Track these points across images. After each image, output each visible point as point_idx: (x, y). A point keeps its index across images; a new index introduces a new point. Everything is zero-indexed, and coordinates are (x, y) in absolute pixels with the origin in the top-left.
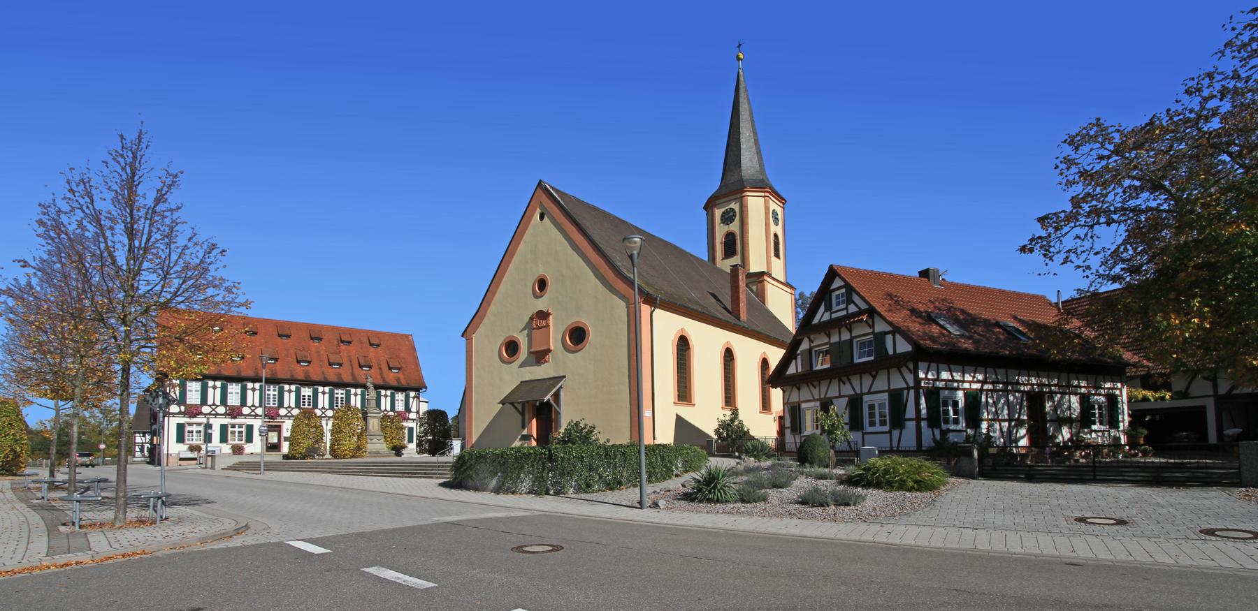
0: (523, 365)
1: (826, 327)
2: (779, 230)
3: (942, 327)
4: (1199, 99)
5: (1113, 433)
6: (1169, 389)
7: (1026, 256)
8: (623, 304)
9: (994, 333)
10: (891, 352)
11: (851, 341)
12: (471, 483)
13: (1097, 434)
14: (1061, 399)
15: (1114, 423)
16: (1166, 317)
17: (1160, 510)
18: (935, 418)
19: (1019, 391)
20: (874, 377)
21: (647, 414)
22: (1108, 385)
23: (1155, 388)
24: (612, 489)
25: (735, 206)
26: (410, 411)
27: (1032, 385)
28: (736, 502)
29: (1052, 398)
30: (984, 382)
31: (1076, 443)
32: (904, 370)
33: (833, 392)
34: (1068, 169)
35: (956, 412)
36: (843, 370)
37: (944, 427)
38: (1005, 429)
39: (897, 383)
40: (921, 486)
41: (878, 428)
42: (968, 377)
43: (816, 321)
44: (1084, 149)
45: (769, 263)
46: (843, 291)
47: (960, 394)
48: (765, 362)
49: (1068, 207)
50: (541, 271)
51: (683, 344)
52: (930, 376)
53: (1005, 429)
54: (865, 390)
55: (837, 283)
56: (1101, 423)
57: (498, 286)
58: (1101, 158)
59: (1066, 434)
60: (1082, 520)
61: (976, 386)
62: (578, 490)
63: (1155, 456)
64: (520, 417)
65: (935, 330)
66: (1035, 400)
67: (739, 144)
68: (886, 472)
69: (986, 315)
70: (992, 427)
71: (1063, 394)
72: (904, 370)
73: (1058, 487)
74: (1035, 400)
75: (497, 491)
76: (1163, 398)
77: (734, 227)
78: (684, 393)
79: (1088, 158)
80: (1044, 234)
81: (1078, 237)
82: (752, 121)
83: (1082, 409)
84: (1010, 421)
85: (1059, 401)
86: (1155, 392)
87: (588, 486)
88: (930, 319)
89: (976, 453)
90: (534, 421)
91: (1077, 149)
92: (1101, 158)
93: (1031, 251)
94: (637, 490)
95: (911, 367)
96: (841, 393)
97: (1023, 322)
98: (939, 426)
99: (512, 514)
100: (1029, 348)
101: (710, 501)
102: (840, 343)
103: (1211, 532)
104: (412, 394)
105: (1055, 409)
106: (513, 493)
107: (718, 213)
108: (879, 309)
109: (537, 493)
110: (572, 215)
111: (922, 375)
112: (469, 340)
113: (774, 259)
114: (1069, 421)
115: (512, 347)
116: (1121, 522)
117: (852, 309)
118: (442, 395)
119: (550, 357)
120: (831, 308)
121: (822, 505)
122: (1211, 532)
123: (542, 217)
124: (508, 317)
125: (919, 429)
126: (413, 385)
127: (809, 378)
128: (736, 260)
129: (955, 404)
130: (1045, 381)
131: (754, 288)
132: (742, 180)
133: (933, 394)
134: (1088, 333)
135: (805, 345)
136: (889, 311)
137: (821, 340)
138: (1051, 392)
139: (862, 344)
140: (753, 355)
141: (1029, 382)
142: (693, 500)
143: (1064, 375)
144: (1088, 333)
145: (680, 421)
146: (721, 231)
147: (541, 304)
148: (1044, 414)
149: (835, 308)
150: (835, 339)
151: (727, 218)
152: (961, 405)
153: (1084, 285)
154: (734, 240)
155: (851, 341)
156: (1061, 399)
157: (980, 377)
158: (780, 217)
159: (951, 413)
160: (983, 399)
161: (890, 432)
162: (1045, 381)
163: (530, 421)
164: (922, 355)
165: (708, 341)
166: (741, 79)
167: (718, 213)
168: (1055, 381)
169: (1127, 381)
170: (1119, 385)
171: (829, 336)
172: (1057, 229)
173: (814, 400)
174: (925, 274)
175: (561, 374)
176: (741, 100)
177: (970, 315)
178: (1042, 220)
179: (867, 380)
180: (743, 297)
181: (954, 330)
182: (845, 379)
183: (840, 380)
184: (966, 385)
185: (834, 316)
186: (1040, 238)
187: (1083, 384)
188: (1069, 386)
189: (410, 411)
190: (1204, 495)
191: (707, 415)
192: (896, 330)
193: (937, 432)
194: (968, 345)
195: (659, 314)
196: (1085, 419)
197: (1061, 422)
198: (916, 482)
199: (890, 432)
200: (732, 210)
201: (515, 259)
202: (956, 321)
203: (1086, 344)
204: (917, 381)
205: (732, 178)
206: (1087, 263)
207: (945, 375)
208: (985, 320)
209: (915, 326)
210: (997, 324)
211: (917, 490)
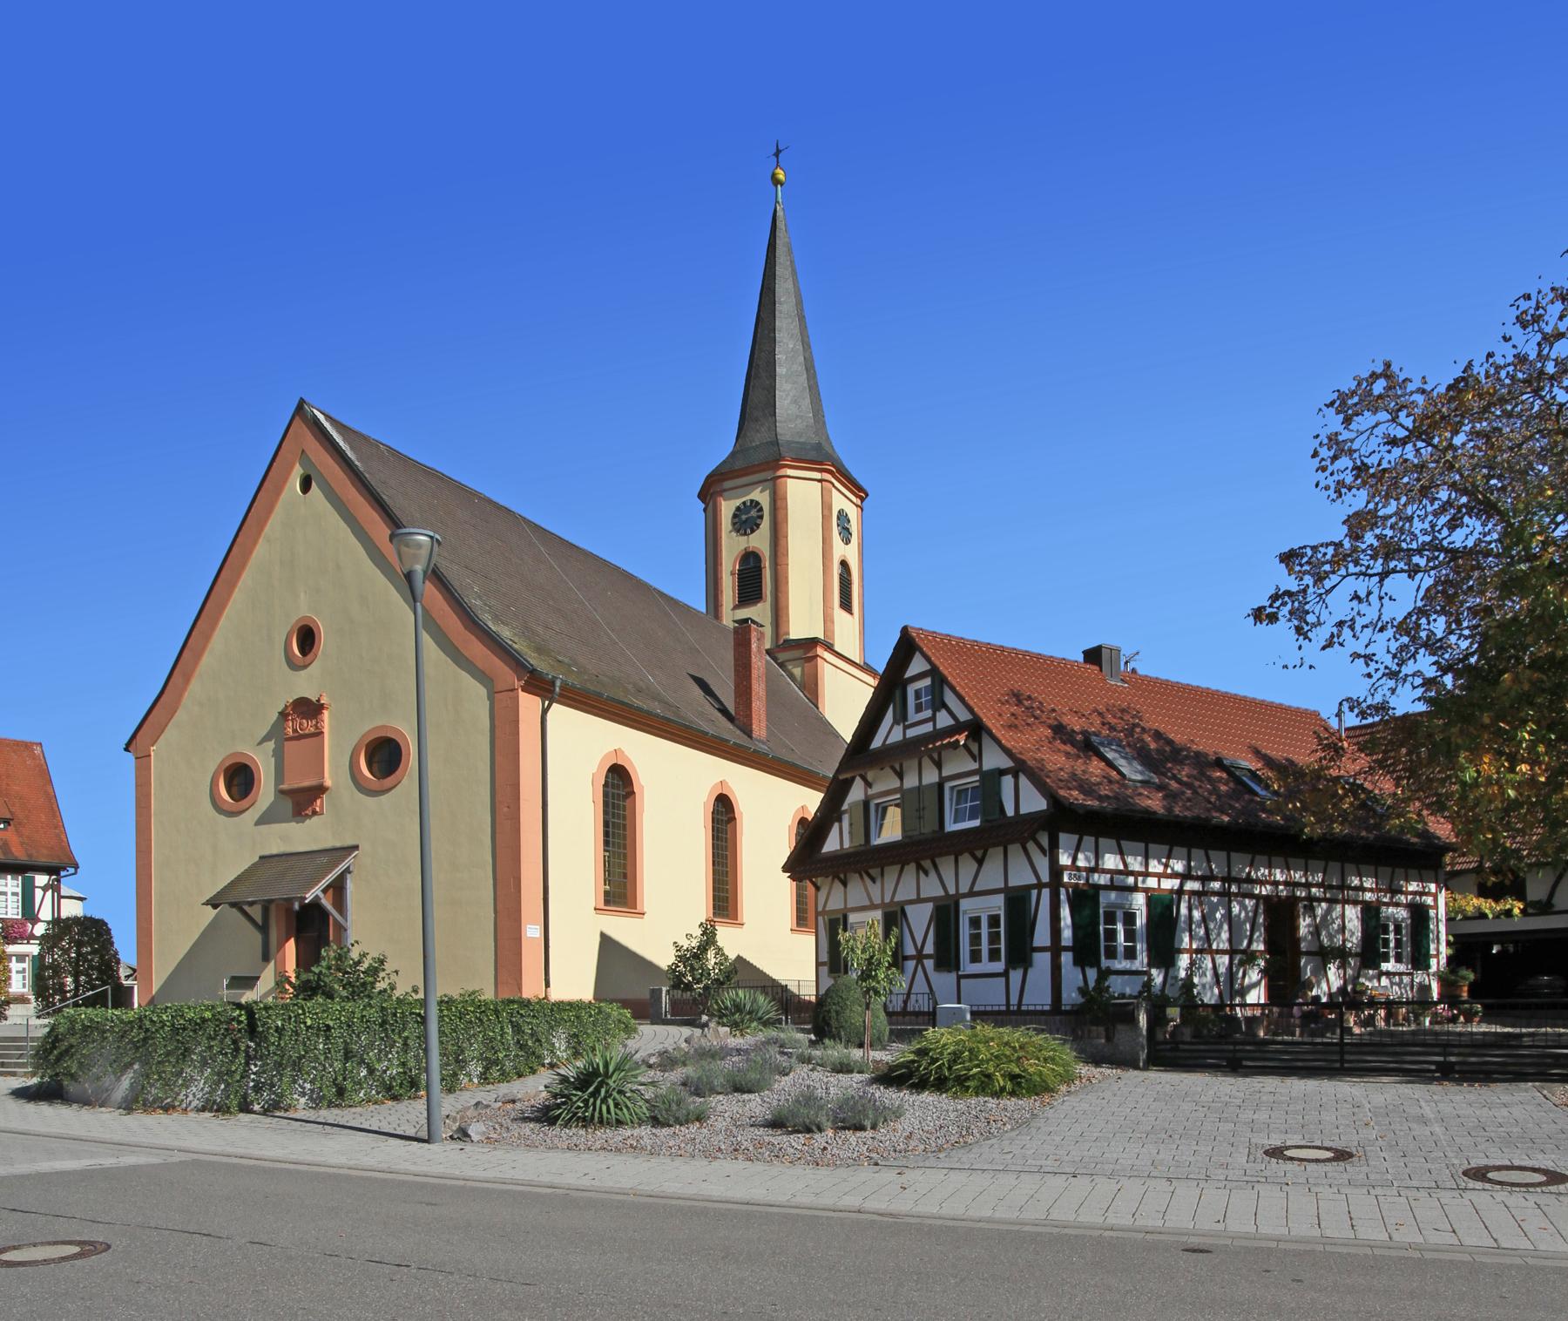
0: (264, 820)
1: (895, 757)
2: (851, 553)
3: (1110, 764)
4: (1539, 337)
5: (1419, 977)
6: (1520, 895)
7: (1263, 627)
8: (483, 692)
9: (1210, 779)
10: (1010, 812)
11: (940, 786)
12: (71, 1087)
13: (1390, 980)
14: (1329, 911)
15: (1419, 960)
16: (1475, 760)
17: (1418, 1130)
18: (1087, 949)
19: (1251, 896)
20: (980, 862)
21: (532, 931)
22: (1413, 886)
23: (1495, 893)
24: (395, 1098)
26: (35, 920)
27: (1276, 883)
28: (641, 1122)
29: (1310, 910)
30: (1185, 877)
31: (1351, 999)
32: (1031, 846)
33: (906, 891)
34: (1335, 458)
35: (1130, 935)
36: (921, 849)
37: (1105, 963)
38: (1222, 970)
39: (1021, 876)
40: (1019, 1085)
41: (986, 966)
42: (1155, 867)
43: (877, 743)
44: (1365, 421)
45: (828, 620)
46: (927, 682)
47: (1139, 900)
49: (1340, 533)
50: (303, 609)
51: (618, 785)
52: (1081, 863)
53: (1222, 970)
54: (964, 889)
55: (917, 666)
56: (1398, 959)
57: (207, 637)
58: (1393, 442)
59: (1334, 978)
60: (1276, 1153)
61: (1169, 884)
62: (317, 1101)
63: (1487, 1018)
65: (1095, 768)
66: (1280, 914)
67: (772, 364)
68: (956, 1057)
69: (1207, 745)
70: (1200, 969)
71: (1332, 902)
72: (1031, 846)
73: (1310, 1085)
74: (1280, 914)
75: (129, 1105)
76: (1508, 913)
77: (759, 541)
78: (620, 889)
79: (1372, 437)
80: (1292, 584)
81: (1356, 597)
82: (802, 318)
83: (1364, 931)
84: (1232, 952)
85: (1324, 917)
86: (1497, 901)
87: (341, 1092)
88: (1088, 747)
89: (1143, 1019)
90: (291, 946)
91: (1347, 421)
92: (1393, 442)
93: (1273, 618)
94: (420, 1105)
96: (918, 890)
97: (1269, 762)
98: (1096, 963)
99: (109, 1162)
100: (1270, 812)
101: (586, 1122)
102: (919, 789)
103: (1479, 1174)
104: (41, 880)
105: (1316, 931)
106: (167, 1109)
107: (727, 508)
108: (988, 722)
109: (221, 1109)
110: (375, 490)
111: (1065, 860)
112: (143, 759)
113: (839, 614)
114: (1341, 954)
115: (240, 778)
116: (1342, 1156)
117: (944, 720)
118: (94, 891)
119: (324, 803)
120: (905, 718)
121: (809, 1130)
122: (1479, 1174)
123: (306, 485)
124: (233, 707)
125: (1056, 968)
126: (43, 860)
127: (868, 861)
128: (759, 612)
129: (1130, 918)
130: (1298, 876)
131: (797, 672)
132: (776, 443)
133: (1085, 899)
134: (1384, 786)
135: (856, 793)
136: (1012, 727)
137: (885, 782)
138: (1311, 899)
139: (961, 794)
141: (1274, 877)
142: (552, 1121)
143: (1334, 866)
144: (1384, 786)
145: (607, 943)
146: (732, 547)
147: (305, 685)
148: (1296, 941)
149: (913, 717)
150: (911, 781)
151: (746, 521)
152: (1141, 920)
153: (1360, 689)
154: (758, 570)
155: (940, 786)
156: (1329, 911)
157: (1179, 866)
158: (854, 527)
159: (1121, 937)
160: (1184, 910)
161: (1005, 974)
162: (1298, 876)
163: (281, 946)
164: (1062, 819)
166: (781, 225)
167: (727, 508)
168: (1319, 877)
169: (1449, 880)
170: (1433, 887)
171: (900, 776)
172: (1319, 579)
173: (873, 907)
174: (1094, 656)
175: (349, 842)
176: (779, 270)
177: (1170, 742)
178: (1288, 558)
179: (968, 866)
180: (759, 688)
181: (1132, 771)
182: (927, 864)
183: (920, 868)
184: (1152, 882)
185: (911, 733)
186: (1288, 593)
187: (1369, 883)
188: (1343, 887)
189: (35, 920)
190: (1506, 1098)
191: (662, 929)
192: (1020, 768)
193: (1092, 974)
194: (1154, 803)
195: (558, 712)
196: (1370, 954)
197: (1325, 955)
198: (1013, 1077)
199: (1005, 974)
200: (755, 504)
201: (246, 579)
202: (1143, 756)
203: (1367, 804)
204: (1056, 871)
205: (758, 437)
206: (1369, 651)
207: (1111, 861)
208: (1198, 754)
209: (1057, 760)
210: (1219, 763)
211: (1013, 1094)
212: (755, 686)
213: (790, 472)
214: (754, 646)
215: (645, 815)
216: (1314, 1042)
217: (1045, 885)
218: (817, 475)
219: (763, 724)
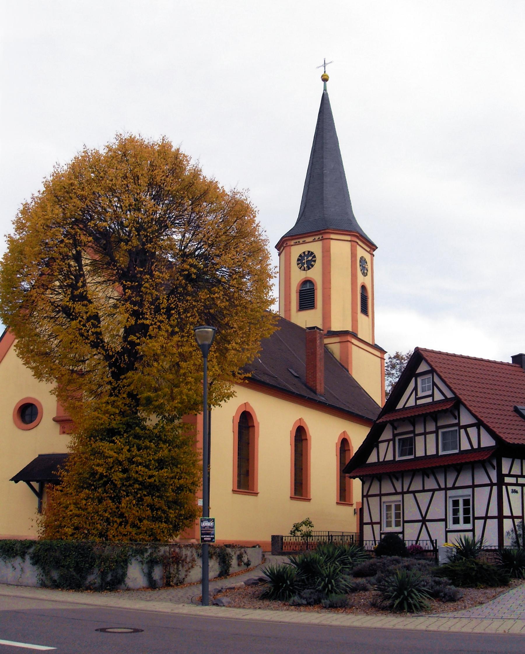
25: (316, 247)
41: (462, 526)
45: (355, 321)
48: (344, 443)
54: (449, 485)
64: (36, 499)
95: (495, 463)
113: (361, 317)
140: (327, 433)
165: (276, 419)
185: (419, 402)
200: (311, 253)
212: (318, 364)
213: (332, 236)
214: (318, 342)
215: (290, 454)
216: (19, 585)
217: (495, 484)
218: (349, 238)
219: (323, 385)
